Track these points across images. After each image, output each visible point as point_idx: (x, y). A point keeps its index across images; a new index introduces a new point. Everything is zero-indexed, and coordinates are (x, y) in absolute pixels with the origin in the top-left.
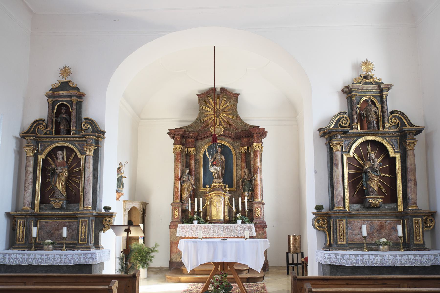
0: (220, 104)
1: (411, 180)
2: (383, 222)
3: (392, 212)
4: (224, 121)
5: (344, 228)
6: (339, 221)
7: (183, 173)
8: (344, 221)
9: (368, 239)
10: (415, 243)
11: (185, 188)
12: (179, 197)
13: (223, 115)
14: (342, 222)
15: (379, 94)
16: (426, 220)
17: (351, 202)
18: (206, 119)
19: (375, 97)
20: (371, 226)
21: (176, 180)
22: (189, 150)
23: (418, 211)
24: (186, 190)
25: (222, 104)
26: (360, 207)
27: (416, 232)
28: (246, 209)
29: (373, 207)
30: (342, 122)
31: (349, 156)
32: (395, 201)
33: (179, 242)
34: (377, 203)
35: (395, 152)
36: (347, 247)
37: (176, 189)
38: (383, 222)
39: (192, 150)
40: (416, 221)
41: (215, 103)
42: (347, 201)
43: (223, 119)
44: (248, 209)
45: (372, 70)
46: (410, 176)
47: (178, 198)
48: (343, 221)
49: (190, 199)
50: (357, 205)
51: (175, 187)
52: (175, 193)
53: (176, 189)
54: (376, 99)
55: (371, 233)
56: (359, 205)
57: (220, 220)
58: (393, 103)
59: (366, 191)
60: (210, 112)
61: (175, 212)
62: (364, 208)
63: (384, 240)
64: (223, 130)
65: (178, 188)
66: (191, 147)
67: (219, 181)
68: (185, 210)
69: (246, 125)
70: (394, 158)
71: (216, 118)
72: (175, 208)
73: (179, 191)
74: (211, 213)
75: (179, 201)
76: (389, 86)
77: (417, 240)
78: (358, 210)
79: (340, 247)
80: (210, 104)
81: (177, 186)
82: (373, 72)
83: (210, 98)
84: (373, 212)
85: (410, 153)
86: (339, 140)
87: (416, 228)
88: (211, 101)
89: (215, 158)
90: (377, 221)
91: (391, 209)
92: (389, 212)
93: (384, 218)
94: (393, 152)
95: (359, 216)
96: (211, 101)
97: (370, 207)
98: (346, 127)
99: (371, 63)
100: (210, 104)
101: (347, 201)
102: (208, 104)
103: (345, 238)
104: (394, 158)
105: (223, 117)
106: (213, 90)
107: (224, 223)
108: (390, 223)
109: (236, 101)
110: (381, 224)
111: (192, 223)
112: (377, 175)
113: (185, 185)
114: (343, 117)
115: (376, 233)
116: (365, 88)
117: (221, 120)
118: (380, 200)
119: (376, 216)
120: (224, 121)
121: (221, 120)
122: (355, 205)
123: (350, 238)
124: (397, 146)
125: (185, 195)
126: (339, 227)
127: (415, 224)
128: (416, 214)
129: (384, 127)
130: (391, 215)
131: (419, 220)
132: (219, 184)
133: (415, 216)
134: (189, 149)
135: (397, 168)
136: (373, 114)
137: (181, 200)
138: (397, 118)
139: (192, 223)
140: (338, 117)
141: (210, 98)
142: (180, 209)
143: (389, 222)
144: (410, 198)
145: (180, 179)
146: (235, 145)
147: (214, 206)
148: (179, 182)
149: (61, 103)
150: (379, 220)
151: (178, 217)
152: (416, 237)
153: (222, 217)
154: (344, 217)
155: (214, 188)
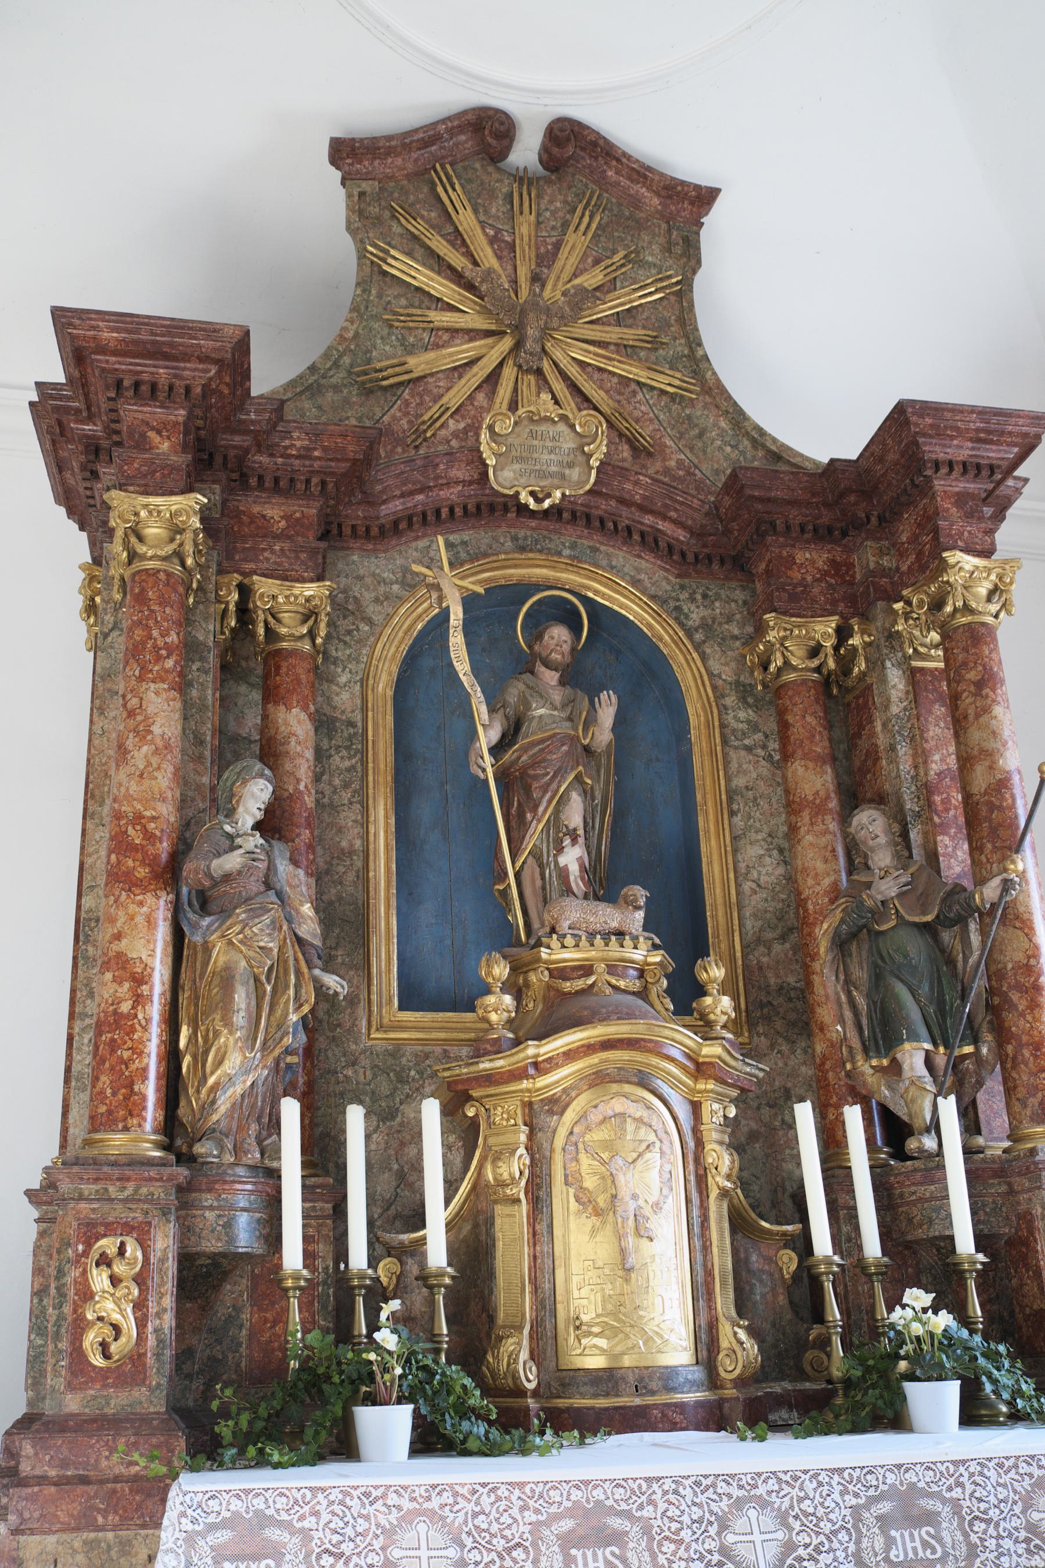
0: (546, 258)
7: (203, 808)
11: (227, 980)
12: (150, 1090)
18: (419, 363)
21: (120, 879)
22: (260, 604)
24: (241, 998)
25: (568, 259)
28: (965, 1242)
33: (338, 168)
37: (109, 989)
39: (289, 599)
41: (505, 249)
44: (981, 1243)
47: (133, 1106)
49: (291, 1111)
51: (91, 944)
52: (98, 1040)
53: (109, 989)
57: (649, 1378)
61: (99, 1280)
65: (140, 980)
66: (304, 581)
67: (609, 916)
68: (216, 1258)
69: (778, 455)
71: (509, 372)
72: (91, 1232)
73: (155, 1010)
74: (546, 1305)
75: (143, 1137)
80: (457, 239)
81: (135, 948)
96: (466, 219)
106: (486, 130)
107: (714, 1418)
109: (688, 253)
111: (344, 1446)
113: (239, 946)
125: (234, 1070)
132: (614, 950)
134: (264, 586)
137: (171, 1125)
139: (344, 1446)
142: (165, 1241)
145: (170, 873)
146: (696, 615)
147: (585, 1199)
148: (158, 907)
151: (136, 1357)
153: (677, 1351)
155: (555, 998)
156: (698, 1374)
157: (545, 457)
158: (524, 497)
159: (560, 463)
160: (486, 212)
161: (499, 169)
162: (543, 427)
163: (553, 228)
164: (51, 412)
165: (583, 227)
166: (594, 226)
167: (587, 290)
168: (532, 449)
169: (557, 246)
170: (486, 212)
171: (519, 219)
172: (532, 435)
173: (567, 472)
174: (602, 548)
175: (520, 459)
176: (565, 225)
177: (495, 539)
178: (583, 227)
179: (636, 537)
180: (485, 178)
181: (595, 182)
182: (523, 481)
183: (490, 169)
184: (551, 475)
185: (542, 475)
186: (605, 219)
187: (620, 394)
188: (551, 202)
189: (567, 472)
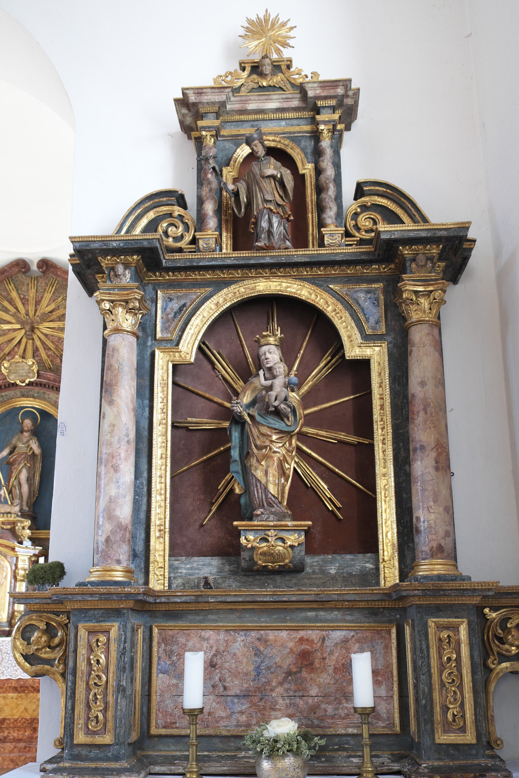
0: (38, 303)
1: (422, 448)
2: (314, 635)
3: (350, 592)
4: (47, 348)
5: (112, 668)
6: (91, 632)
8: (114, 633)
9: (243, 718)
10: (443, 738)
13: (45, 331)
14: (103, 638)
15: (308, 128)
16: (504, 628)
17: (175, 550)
19: (295, 139)
20: (258, 653)
23: (447, 585)
26: (220, 571)
27: (442, 685)
29: (265, 571)
30: (166, 233)
31: (177, 358)
32: (370, 544)
34: (280, 548)
35: (368, 338)
36: (117, 758)
38: (314, 635)
40: (444, 634)
41: (25, 301)
42: (159, 546)
43: (43, 343)
45: (285, 45)
46: (421, 434)
48: (107, 632)
50: (207, 560)
54: (298, 144)
55: (258, 689)
56: (215, 562)
58: (360, 159)
59: (243, 501)
60: (9, 323)
62: (234, 573)
63: (283, 727)
64: (35, 368)
70: (364, 365)
71: (24, 340)
76: (467, 225)
77: (447, 728)
78: (207, 584)
79: (86, 759)
80: (11, 302)
82: (286, 53)
83: (11, 287)
84: (265, 592)
85: (418, 335)
86: (124, 288)
87: (442, 668)
88: (14, 294)
89: (14, 448)
90: (284, 634)
91: (347, 579)
92: (335, 591)
93: (316, 620)
94: (357, 337)
95: (210, 611)
96: (14, 294)
97: (254, 571)
98: (180, 250)
99: (284, 25)
100: (11, 302)
101: (159, 546)
102: (6, 304)
103: (110, 714)
104: (364, 365)
105: (43, 337)
108: (346, 641)
110: (305, 647)
112: (281, 432)
114: (170, 215)
115: (280, 690)
116: (251, 106)
117: (38, 343)
118: (294, 539)
119: (280, 609)
120: (47, 348)
121: (38, 343)
122: (198, 561)
123: (166, 714)
124: (374, 314)
126: (89, 664)
127: (440, 650)
128: (445, 601)
129: (321, 244)
130: (348, 607)
131: (456, 628)
133: (438, 610)
135: (376, 402)
136: (269, 186)
138: (380, 213)
140: (151, 215)
141: (11, 287)
143: (337, 635)
144: (423, 526)
149: (28, 409)
150: (296, 629)
152: (445, 709)
154: (116, 613)
156: (7, 624)
157: (21, 371)
158: (18, 382)
159: (26, 373)
160: (21, 290)
161: (26, 276)
162: (18, 364)
163: (41, 292)
164: (316, 73)
165: (49, 291)
166: (53, 290)
167: (46, 314)
168: (17, 370)
169: (42, 298)
170: (21, 290)
171: (30, 291)
172: (16, 366)
173: (29, 375)
174: (47, 392)
175: (14, 373)
176: (45, 290)
177: (15, 393)
178: (49, 291)
179: (55, 389)
180: (22, 279)
181: (55, 275)
182: (17, 378)
183: (23, 276)
184: (25, 376)
185: (22, 376)
186: (57, 287)
187: (58, 342)
188: (41, 284)
189: (29, 375)
